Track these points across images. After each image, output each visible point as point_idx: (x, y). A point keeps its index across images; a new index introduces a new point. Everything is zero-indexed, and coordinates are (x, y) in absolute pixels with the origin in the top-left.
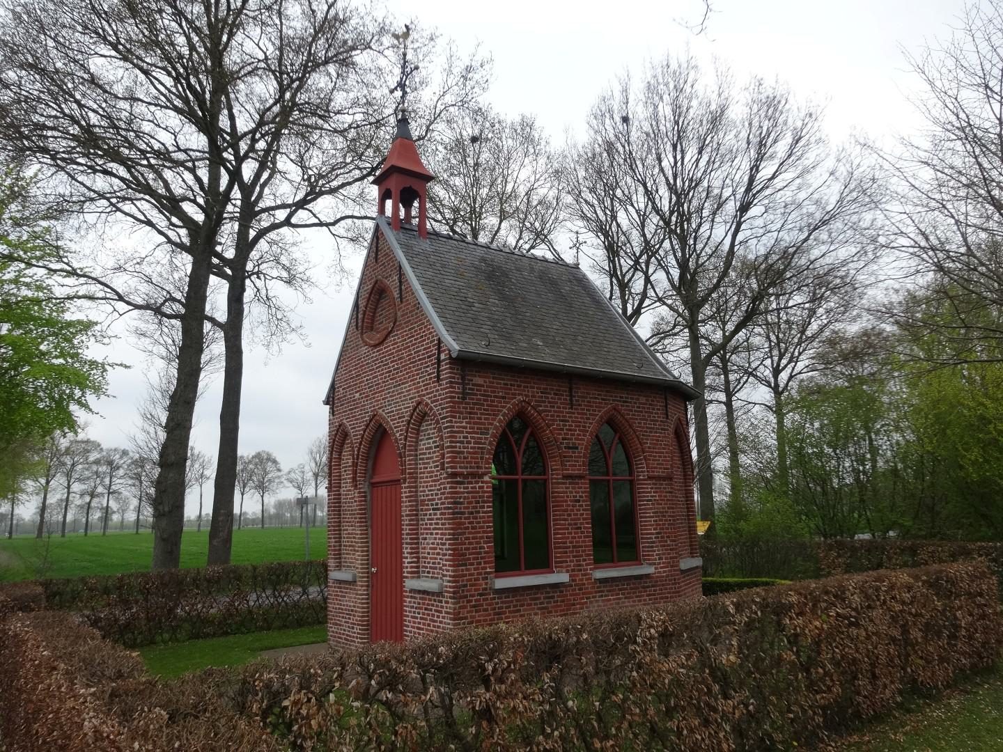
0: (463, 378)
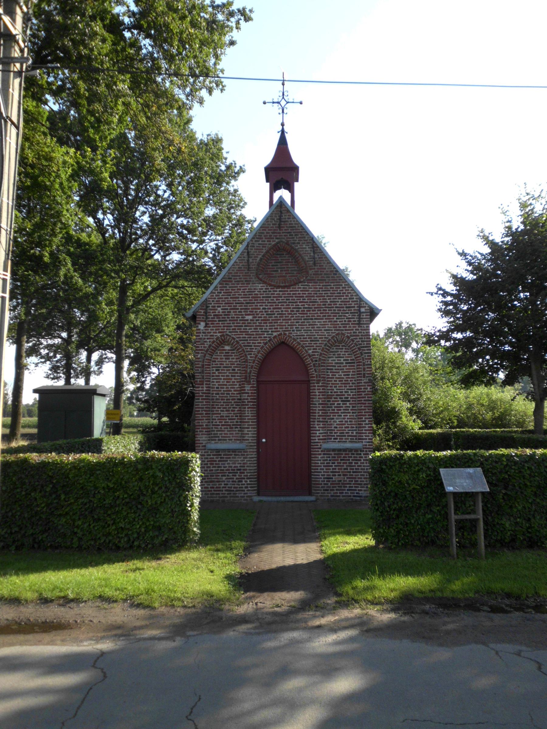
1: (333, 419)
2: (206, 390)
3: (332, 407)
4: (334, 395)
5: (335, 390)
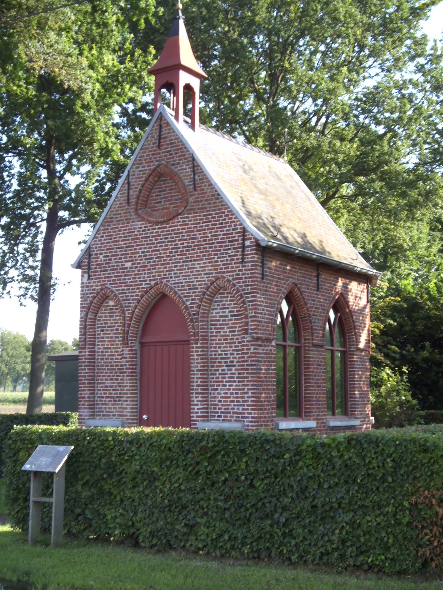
0: (263, 263)
1: (217, 390)
2: (89, 355)
3: (215, 374)
4: (217, 358)
5: (220, 352)
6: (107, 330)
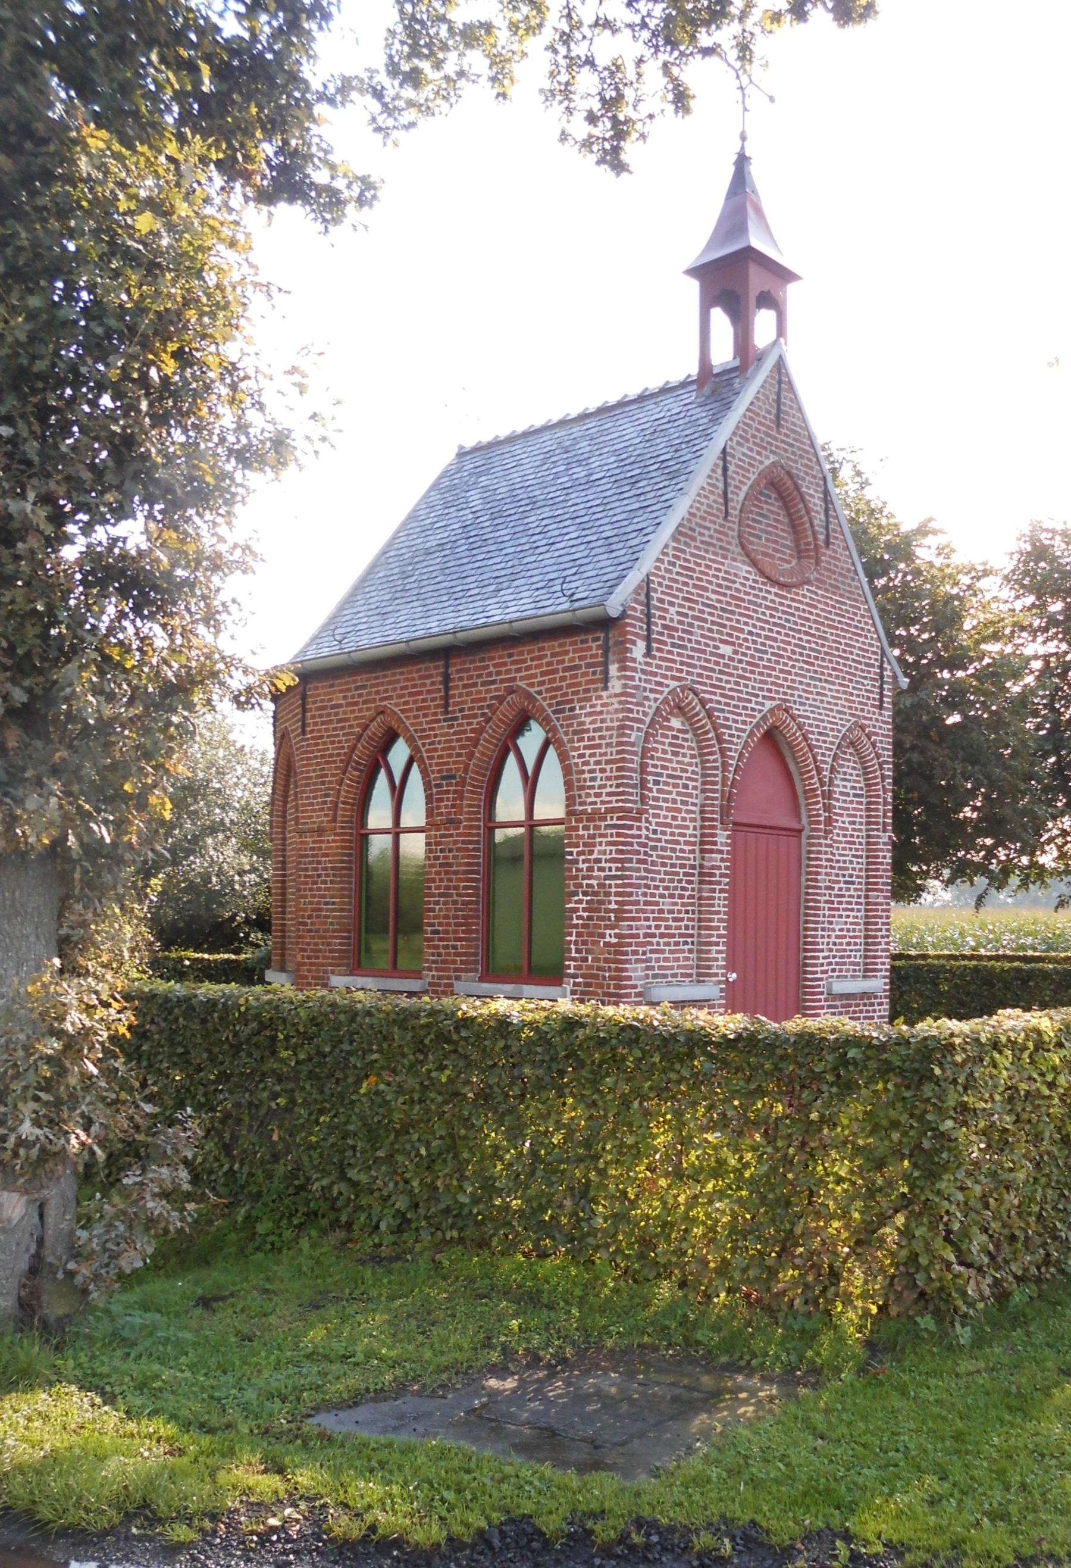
6: (666, 784)
